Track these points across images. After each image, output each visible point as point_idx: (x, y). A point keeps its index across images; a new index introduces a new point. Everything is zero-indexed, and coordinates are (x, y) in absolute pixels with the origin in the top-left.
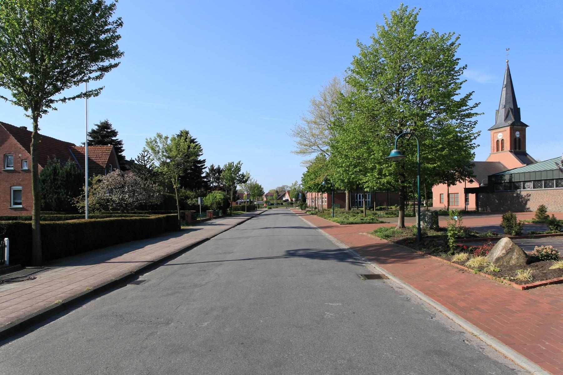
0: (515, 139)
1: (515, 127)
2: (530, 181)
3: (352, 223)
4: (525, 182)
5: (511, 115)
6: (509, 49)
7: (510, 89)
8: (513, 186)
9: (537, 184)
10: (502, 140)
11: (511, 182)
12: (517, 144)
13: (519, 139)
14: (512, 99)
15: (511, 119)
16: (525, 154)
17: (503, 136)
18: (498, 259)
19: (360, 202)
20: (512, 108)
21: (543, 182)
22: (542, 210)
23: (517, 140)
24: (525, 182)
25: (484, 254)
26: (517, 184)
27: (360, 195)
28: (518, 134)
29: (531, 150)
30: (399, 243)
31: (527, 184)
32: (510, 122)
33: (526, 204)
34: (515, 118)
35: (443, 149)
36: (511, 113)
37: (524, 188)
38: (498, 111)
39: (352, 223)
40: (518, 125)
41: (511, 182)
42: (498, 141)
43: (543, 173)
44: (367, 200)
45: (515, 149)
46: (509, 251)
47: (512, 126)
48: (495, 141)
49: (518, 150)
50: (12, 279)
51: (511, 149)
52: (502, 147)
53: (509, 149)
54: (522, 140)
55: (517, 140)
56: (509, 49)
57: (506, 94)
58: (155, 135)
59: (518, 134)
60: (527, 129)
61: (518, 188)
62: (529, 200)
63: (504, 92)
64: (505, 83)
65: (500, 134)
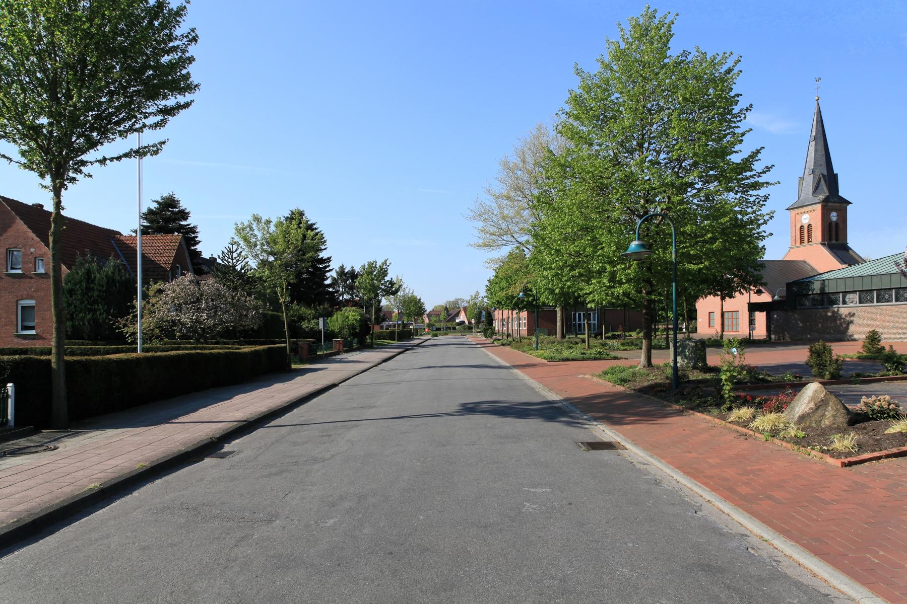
0: (830, 224)
1: (830, 204)
2: (854, 292)
3: (567, 360)
4: (845, 293)
5: (823, 186)
6: (820, 79)
7: (822, 143)
8: (827, 299)
9: (865, 296)
10: (809, 225)
11: (823, 293)
12: (834, 233)
13: (837, 224)
14: (824, 159)
15: (823, 192)
16: (846, 248)
17: (811, 219)
18: (802, 418)
19: (580, 325)
20: (826, 173)
21: (875, 292)
22: (873, 338)
23: (834, 225)
24: (845, 293)
25: (779, 409)
26: (833, 297)
27: (580, 315)
28: (834, 216)
29: (855, 241)
30: (643, 391)
31: (848, 296)
32: (822, 197)
33: (847, 328)
34: (829, 191)
35: (713, 240)
36: (822, 182)
37: (844, 302)
38: (802, 179)
39: (567, 360)
40: (834, 202)
41: (823, 293)
42: (802, 227)
43: (875, 279)
44: (592, 322)
45: (830, 239)
46: (821, 405)
47: (825, 203)
48: (798, 227)
49: (834, 242)
50: (20, 449)
51: (823, 240)
52: (809, 236)
53: (820, 240)
54: (841, 225)
55: (834, 225)
56: (820, 79)
57: (816, 151)
58: (250, 218)
59: (834, 216)
60: (849, 207)
61: (834, 302)
62: (852, 322)
63: (812, 149)
64: (814, 134)
65: (806, 216)
